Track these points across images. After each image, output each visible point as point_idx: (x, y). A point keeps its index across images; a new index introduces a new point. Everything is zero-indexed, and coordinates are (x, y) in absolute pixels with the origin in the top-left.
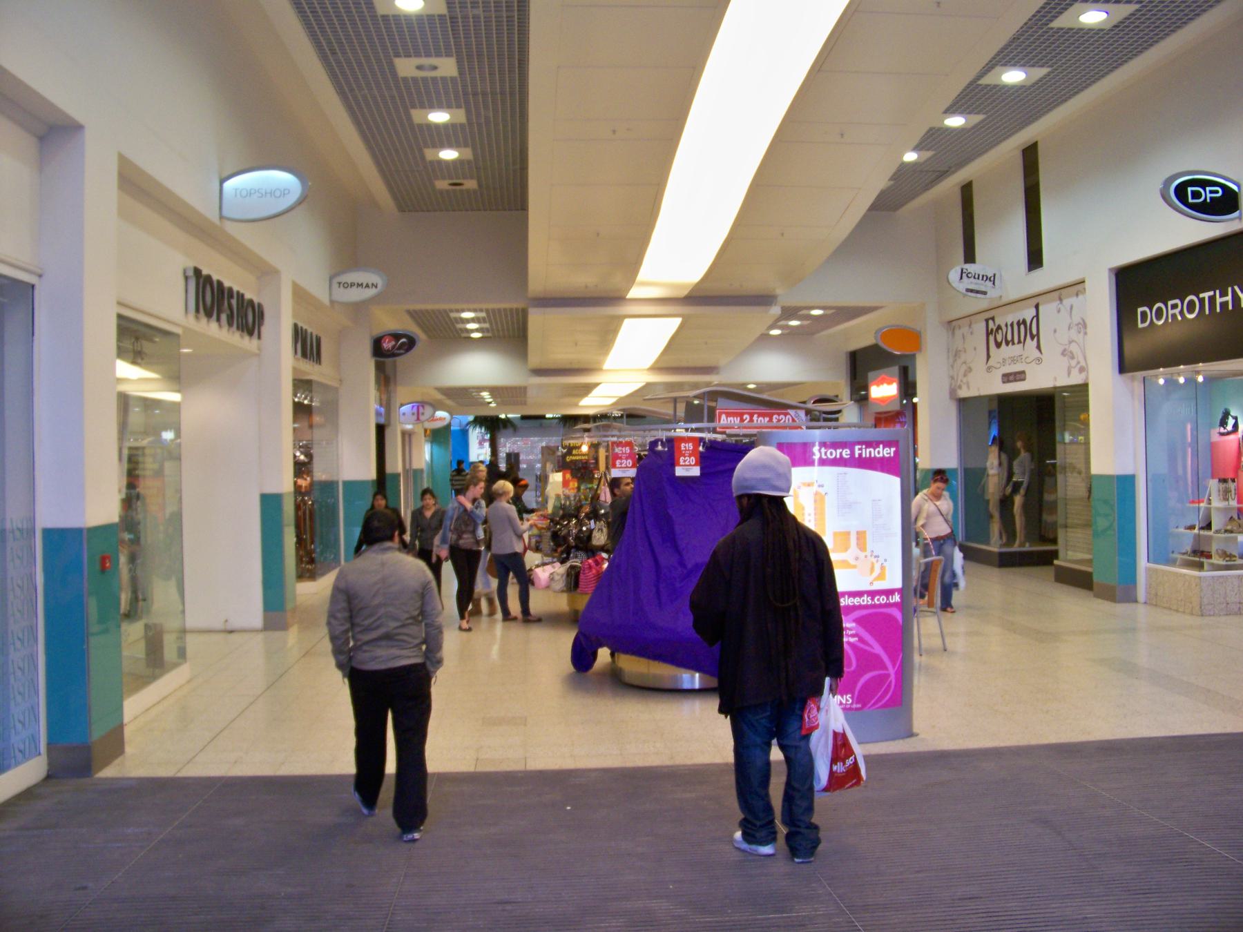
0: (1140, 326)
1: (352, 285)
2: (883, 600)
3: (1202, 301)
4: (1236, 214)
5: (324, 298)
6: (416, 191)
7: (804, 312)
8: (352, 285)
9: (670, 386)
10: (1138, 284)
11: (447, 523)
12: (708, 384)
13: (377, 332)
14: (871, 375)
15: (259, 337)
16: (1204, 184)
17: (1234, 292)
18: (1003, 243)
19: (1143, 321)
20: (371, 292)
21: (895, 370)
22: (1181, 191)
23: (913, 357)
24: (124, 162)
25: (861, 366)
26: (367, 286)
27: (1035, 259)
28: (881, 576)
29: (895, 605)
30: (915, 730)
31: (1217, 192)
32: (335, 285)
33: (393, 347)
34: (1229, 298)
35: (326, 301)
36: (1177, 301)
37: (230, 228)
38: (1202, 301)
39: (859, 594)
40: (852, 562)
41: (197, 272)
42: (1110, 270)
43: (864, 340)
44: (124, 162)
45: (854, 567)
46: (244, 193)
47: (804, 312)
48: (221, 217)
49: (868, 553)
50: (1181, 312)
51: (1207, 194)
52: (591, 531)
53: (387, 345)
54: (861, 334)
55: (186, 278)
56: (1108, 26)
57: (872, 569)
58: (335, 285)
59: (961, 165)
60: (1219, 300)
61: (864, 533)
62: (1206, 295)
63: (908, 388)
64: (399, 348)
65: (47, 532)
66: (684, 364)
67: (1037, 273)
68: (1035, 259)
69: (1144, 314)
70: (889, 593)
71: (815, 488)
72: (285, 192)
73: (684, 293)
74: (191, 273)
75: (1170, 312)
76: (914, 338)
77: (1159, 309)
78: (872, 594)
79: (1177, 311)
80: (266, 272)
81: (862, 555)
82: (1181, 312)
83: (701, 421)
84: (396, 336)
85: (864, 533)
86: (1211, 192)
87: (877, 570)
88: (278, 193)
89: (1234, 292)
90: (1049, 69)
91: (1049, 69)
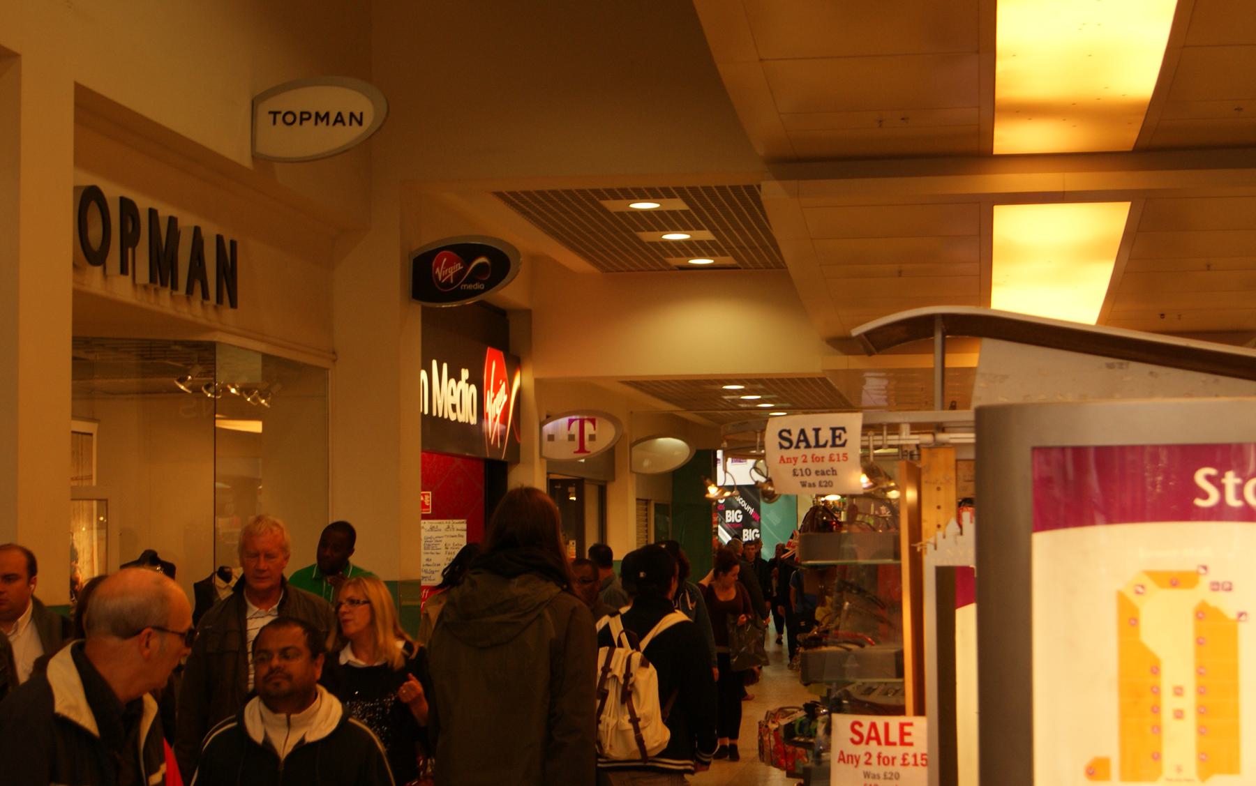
1: (304, 117)
5: (235, 149)
8: (304, 117)
11: (284, 662)
12: (489, 388)
13: (428, 238)
20: (347, 135)
26: (339, 119)
32: (264, 119)
33: (458, 275)
35: (247, 162)
42: (76, 188)
52: (607, 627)
53: (445, 271)
58: (264, 119)
64: (471, 280)
65: (942, 572)
71: (1202, 592)
73: (1127, 137)
83: (929, 405)
84: (466, 251)
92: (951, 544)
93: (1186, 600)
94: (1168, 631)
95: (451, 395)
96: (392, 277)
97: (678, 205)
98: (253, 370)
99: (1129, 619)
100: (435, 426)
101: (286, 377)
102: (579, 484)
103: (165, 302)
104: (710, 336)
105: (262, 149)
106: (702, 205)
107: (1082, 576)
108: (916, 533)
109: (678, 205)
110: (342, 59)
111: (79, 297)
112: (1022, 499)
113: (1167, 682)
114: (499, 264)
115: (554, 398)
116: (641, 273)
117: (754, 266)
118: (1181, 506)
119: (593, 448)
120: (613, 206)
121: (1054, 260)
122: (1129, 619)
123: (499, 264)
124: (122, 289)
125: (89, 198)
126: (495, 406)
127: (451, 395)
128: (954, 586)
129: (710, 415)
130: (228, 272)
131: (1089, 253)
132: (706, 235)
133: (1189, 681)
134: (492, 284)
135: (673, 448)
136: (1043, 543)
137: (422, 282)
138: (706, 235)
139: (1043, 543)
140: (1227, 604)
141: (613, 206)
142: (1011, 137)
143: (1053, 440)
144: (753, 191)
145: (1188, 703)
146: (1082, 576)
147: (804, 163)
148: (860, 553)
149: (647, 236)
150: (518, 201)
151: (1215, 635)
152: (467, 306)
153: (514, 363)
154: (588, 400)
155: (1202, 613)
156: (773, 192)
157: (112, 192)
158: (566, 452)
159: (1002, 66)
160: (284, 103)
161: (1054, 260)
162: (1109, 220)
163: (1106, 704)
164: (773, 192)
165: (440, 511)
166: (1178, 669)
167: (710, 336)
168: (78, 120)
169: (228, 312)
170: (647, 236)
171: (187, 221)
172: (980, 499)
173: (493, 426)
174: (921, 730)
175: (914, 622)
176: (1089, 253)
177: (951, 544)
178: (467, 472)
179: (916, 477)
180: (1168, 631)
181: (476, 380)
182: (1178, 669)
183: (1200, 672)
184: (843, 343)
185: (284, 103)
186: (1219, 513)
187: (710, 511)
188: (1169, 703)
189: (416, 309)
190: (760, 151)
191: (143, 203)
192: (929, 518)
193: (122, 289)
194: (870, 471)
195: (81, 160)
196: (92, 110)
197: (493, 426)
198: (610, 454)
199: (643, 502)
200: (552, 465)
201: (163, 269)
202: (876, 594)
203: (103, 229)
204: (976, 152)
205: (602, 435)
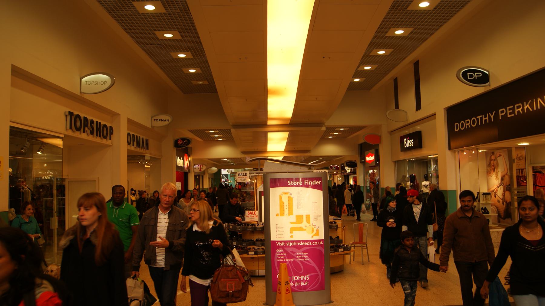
0: (456, 130)
1: (160, 120)
2: (316, 243)
3: (477, 119)
4: (488, 83)
5: (149, 126)
6: (187, 86)
7: (337, 129)
8: (160, 120)
9: (297, 157)
10: (455, 113)
13: (177, 137)
14: (366, 153)
15: (110, 139)
16: (474, 71)
17: (489, 115)
18: (408, 101)
19: (457, 128)
21: (373, 151)
22: (464, 75)
23: (378, 145)
24: (13, 66)
25: (363, 149)
27: (419, 107)
28: (317, 234)
29: (321, 245)
30: (332, 300)
31: (480, 75)
32: (153, 120)
34: (487, 118)
36: (469, 120)
37: (86, 96)
38: (477, 119)
39: (307, 241)
40: (304, 228)
41: (71, 114)
43: (362, 141)
44: (13, 66)
45: (305, 230)
46: (89, 83)
47: (337, 129)
48: (81, 93)
49: (311, 224)
50: (470, 124)
51: (475, 76)
53: (180, 143)
54: (361, 137)
55: (66, 116)
56: (432, 9)
57: (313, 231)
58: (153, 120)
59: (390, 71)
60: (484, 119)
61: (309, 215)
62: (479, 117)
63: (377, 158)
66: (296, 149)
67: (419, 111)
68: (419, 107)
69: (457, 125)
70: (319, 241)
71: (289, 195)
72: (105, 83)
73: (288, 122)
74: (67, 114)
75: (466, 125)
76: (378, 139)
77: (462, 123)
78: (312, 241)
79: (469, 124)
80: (114, 115)
81: (308, 225)
82: (470, 124)
84: (183, 139)
85: (309, 215)
86: (477, 75)
87: (315, 231)
88: (102, 83)
89: (489, 115)
90: (413, 29)
91: (413, 29)
92: (261, 188)
93: (287, 196)
94: (285, 199)
95: (180, 162)
96: (172, 144)
97: (217, 131)
98: (149, 158)
99: (281, 198)
100: (178, 167)
101: (153, 160)
102: (199, 176)
103: (138, 150)
104: (222, 151)
105: (153, 125)
106: (221, 132)
107: (275, 193)
108: (256, 187)
109: (217, 131)
110: (164, 111)
111: (128, 150)
112: (269, 184)
113: (285, 205)
114: (189, 141)
115: (195, 162)
116: (211, 141)
117: (229, 140)
118: (286, 185)
119: (202, 170)
120: (207, 132)
121: (277, 144)
122: (281, 198)
123: (189, 141)
124: (132, 148)
125: (129, 134)
126: (186, 163)
127: (180, 162)
128: (261, 193)
129: (220, 163)
130: (147, 144)
131: (283, 139)
132: (221, 136)
133: (287, 204)
134: (187, 145)
135: (215, 169)
136: (271, 189)
137: (176, 144)
138: (221, 136)
139: (271, 189)
140: (292, 196)
141: (207, 132)
142: (270, 122)
143: (272, 178)
144: (230, 130)
145: (287, 207)
146: (275, 193)
147: (237, 126)
148: (248, 189)
149: (212, 136)
150: (192, 131)
151: (290, 199)
152: (183, 147)
153: (189, 156)
154: (201, 162)
155: (289, 197)
156: (233, 130)
157: (131, 133)
158: (198, 171)
159: (268, 113)
160: (156, 118)
161: (277, 144)
162: (286, 135)
163: (278, 207)
164: (233, 130)
165: (177, 181)
166: (286, 203)
167: (222, 151)
168: (128, 123)
169: (147, 151)
170: (212, 136)
171: (141, 137)
172: (264, 182)
173: (186, 166)
174: (257, 212)
175: (256, 198)
176: (283, 139)
177: (261, 188)
178: (183, 175)
179: (256, 179)
180: (285, 199)
181: (183, 159)
182: (286, 203)
183: (289, 204)
184: (244, 153)
185: (156, 118)
186: (291, 186)
187: (220, 179)
188: (285, 207)
189: (175, 148)
190: (231, 124)
191: (136, 135)
192: (258, 185)
193: (132, 148)
194: (250, 179)
195: (128, 129)
196: (130, 121)
197: (186, 166)
198: (204, 171)
199: (209, 178)
200: (195, 173)
201: (138, 145)
202: (251, 195)
203: (132, 139)
204: (265, 125)
205: (204, 168)
